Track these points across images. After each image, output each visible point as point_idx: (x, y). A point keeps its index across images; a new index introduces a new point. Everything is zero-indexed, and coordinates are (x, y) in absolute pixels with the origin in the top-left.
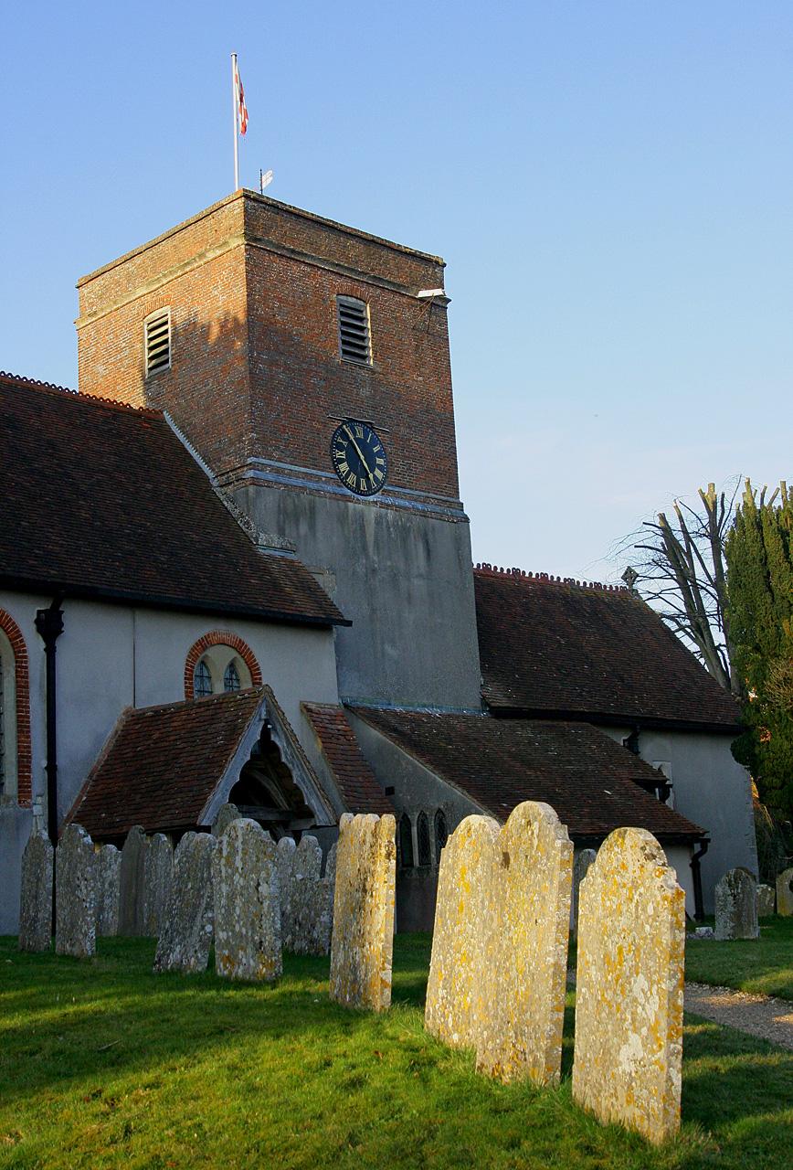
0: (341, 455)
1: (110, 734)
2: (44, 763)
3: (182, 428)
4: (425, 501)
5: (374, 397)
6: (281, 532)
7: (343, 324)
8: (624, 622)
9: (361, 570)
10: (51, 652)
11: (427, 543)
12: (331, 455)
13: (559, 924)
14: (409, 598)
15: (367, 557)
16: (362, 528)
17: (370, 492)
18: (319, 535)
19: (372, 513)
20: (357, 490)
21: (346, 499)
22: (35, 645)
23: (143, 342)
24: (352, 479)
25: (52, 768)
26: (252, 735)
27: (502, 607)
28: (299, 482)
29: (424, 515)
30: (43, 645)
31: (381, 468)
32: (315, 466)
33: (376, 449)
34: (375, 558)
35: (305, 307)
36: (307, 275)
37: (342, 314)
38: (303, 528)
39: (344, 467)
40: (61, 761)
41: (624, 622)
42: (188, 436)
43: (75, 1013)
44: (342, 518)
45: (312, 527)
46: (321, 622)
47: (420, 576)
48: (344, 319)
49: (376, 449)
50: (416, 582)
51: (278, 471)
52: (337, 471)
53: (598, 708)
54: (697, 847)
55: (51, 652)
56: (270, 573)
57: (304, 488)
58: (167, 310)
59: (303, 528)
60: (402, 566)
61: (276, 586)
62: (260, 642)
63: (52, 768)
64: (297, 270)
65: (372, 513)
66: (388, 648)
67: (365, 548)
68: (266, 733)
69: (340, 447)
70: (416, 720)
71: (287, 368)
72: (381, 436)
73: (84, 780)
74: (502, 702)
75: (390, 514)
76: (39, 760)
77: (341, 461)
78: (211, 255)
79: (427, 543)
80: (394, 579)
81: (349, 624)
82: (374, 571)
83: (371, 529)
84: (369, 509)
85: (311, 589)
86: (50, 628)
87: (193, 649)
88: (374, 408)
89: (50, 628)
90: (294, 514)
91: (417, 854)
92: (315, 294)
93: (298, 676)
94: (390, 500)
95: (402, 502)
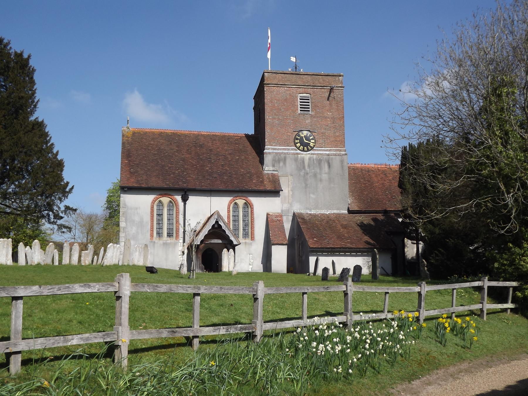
5: (311, 122)
6: (273, 166)
9: (302, 174)
10: (185, 204)
12: (294, 142)
13: (518, 326)
14: (321, 180)
16: (303, 162)
17: (308, 150)
20: (303, 150)
21: (298, 154)
22: (181, 204)
24: (301, 147)
25: (184, 232)
28: (281, 151)
29: (328, 155)
31: (312, 139)
32: (288, 146)
34: (308, 170)
37: (300, 99)
39: (298, 145)
43: (372, 288)
44: (296, 160)
45: (285, 163)
46: (275, 192)
48: (301, 104)
51: (274, 149)
52: (296, 147)
55: (185, 204)
57: (282, 153)
59: (281, 164)
60: (318, 171)
62: (255, 201)
64: (282, 89)
66: (312, 195)
67: (304, 167)
68: (217, 222)
69: (297, 139)
70: (257, 153)
71: (279, 119)
75: (315, 156)
76: (181, 230)
77: (297, 143)
80: (315, 175)
82: (307, 174)
84: (306, 156)
90: (280, 159)
91: (242, 230)
92: (290, 95)
94: (316, 152)
95: (319, 152)
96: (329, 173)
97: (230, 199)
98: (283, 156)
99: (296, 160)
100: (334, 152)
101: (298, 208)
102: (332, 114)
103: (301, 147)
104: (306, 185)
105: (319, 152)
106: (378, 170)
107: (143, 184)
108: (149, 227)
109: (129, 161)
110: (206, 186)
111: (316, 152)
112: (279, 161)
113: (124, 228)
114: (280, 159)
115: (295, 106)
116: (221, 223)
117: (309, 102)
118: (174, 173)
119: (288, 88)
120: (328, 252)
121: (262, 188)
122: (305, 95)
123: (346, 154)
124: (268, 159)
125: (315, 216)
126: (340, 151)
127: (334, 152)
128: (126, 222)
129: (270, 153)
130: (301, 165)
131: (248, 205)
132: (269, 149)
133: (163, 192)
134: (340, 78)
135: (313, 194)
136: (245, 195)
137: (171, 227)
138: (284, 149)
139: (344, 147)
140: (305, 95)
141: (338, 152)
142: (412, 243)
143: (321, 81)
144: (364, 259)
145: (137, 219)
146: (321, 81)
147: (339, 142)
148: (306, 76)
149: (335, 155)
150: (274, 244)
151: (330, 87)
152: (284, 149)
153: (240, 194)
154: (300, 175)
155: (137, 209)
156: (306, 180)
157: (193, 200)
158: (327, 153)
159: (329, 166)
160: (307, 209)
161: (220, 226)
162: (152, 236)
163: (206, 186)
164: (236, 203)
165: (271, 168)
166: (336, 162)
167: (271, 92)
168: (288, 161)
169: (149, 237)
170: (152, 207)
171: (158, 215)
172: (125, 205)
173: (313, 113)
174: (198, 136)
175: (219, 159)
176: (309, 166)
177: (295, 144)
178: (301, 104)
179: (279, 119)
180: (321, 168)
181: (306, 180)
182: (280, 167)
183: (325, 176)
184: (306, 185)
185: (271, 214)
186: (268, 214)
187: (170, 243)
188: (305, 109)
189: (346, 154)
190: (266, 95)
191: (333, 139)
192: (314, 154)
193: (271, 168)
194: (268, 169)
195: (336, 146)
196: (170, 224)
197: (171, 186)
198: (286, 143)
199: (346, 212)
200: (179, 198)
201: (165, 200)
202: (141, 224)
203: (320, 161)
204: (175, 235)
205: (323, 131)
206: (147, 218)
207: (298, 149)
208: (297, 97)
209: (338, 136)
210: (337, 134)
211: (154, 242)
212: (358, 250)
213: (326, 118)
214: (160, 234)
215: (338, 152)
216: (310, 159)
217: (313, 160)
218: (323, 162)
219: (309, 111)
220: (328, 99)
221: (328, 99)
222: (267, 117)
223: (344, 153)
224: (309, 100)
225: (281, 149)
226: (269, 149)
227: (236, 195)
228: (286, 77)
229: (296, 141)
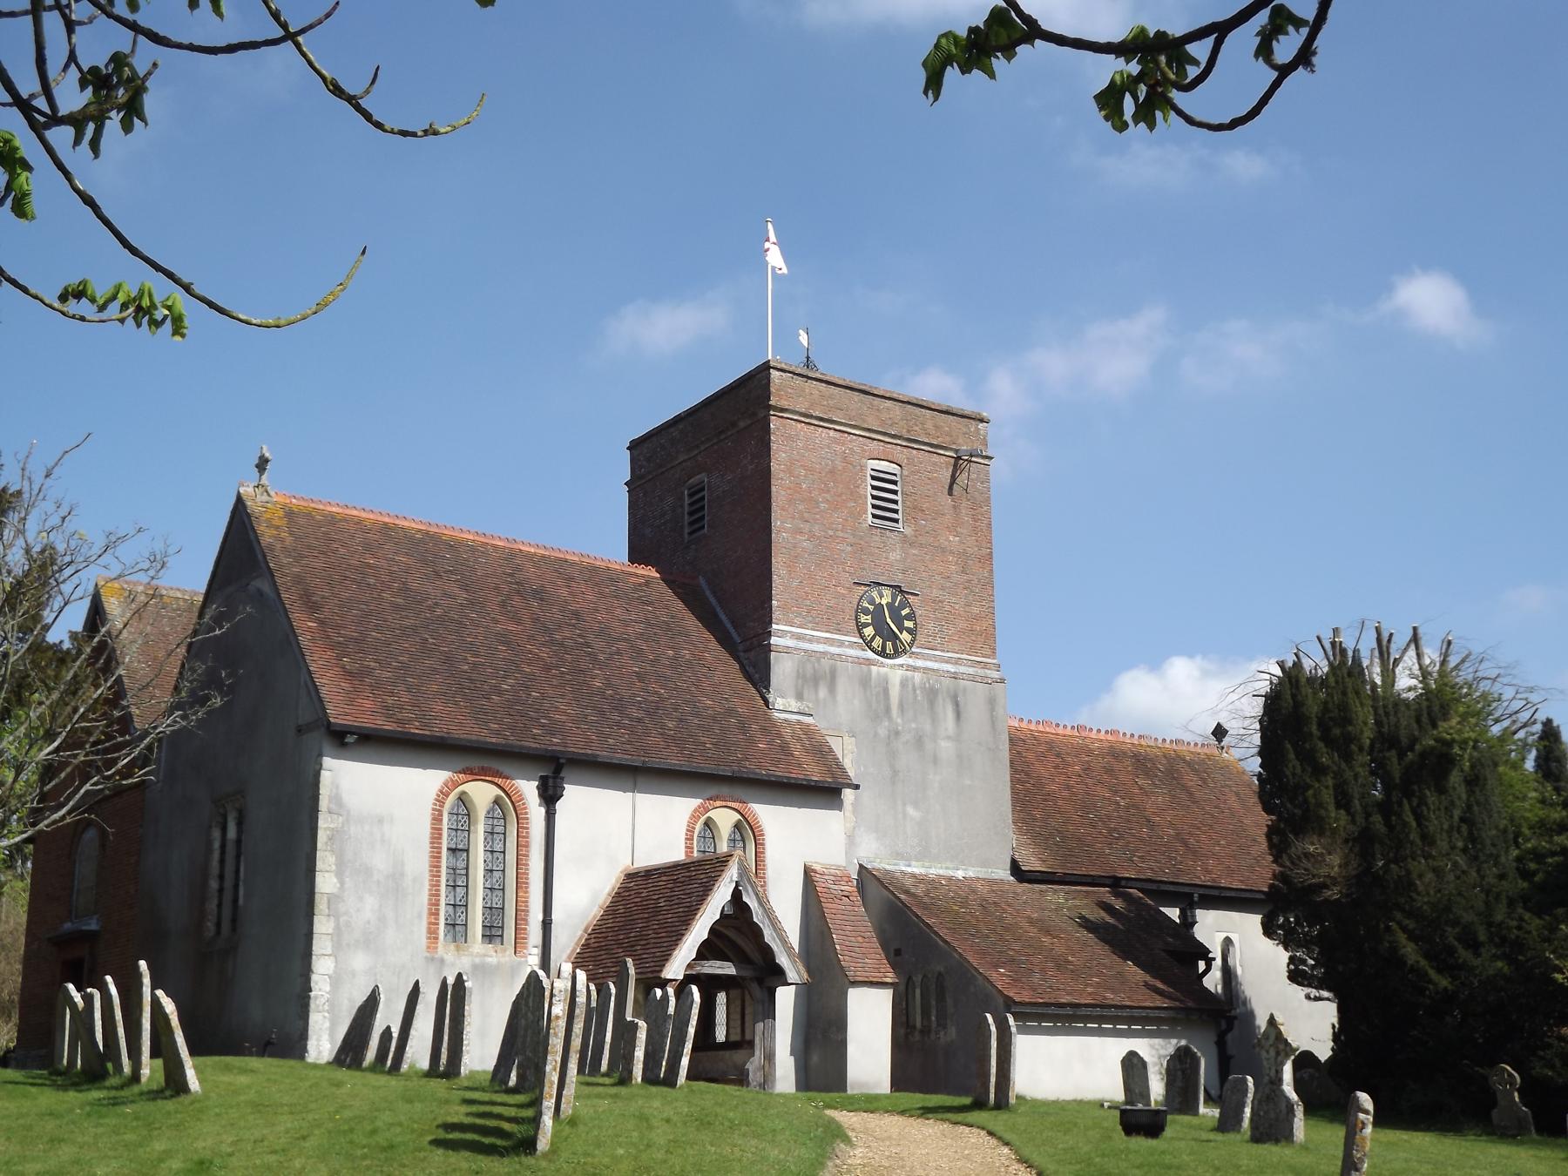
0: (865, 619)
1: (607, 890)
2: (540, 917)
3: (714, 593)
4: (957, 662)
7: (874, 488)
8: (1204, 781)
9: (882, 732)
11: (957, 704)
14: (935, 760)
15: (890, 718)
16: (886, 691)
17: (897, 653)
18: (840, 697)
19: (896, 676)
21: (869, 662)
22: (536, 812)
23: (682, 506)
24: (878, 642)
25: (547, 924)
26: (720, 897)
27: (1057, 767)
28: (820, 648)
29: (955, 676)
30: (543, 810)
31: (909, 631)
32: (839, 631)
33: (904, 613)
35: (832, 472)
36: (835, 441)
37: (873, 478)
38: (823, 692)
39: (869, 631)
40: (556, 915)
41: (1204, 781)
42: (719, 602)
44: (865, 682)
45: (832, 689)
46: (824, 791)
47: (948, 738)
48: (875, 493)
49: (904, 613)
50: (943, 744)
51: (799, 637)
53: (1149, 875)
54: (1224, 1025)
56: (779, 735)
58: (703, 476)
59: (823, 692)
60: (928, 727)
61: (785, 748)
62: (772, 817)
63: (547, 924)
64: (823, 435)
65: (896, 676)
66: (911, 811)
67: (888, 710)
68: (737, 895)
69: (866, 611)
72: (911, 599)
73: (580, 933)
74: (1031, 863)
75: (918, 676)
76: (536, 915)
77: (867, 625)
78: (742, 424)
79: (957, 704)
80: (919, 741)
81: (857, 787)
82: (897, 733)
83: (895, 692)
84: (893, 671)
85: (822, 752)
86: (550, 797)
87: (695, 811)
88: (904, 572)
89: (550, 797)
90: (818, 676)
93: (796, 849)
94: (920, 663)
95: (930, 664)
96: (957, 738)
97: (697, 802)
98: (826, 663)
99: (865, 682)
100: (971, 671)
101: (875, 853)
102: (961, 542)
103: (878, 642)
104: (895, 773)
105: (930, 664)
106: (1035, 738)
107: (410, 721)
108: (424, 898)
109: (321, 622)
110: (625, 752)
111: (920, 663)
112: (815, 680)
113: (332, 899)
114: (818, 676)
115: (856, 496)
116: (749, 900)
117: (895, 492)
118: (500, 693)
119: (838, 435)
120: (1054, 1018)
121: (780, 772)
122: (884, 465)
123: (1002, 681)
124: (782, 670)
125: (932, 884)
126: (985, 666)
127: (971, 671)
128: (340, 874)
129: (787, 650)
130: (877, 699)
131: (746, 830)
132: (783, 634)
133: (476, 763)
134: (981, 426)
135: (916, 805)
136: (739, 791)
137: (496, 903)
138: (827, 641)
139: (993, 654)
140: (884, 465)
141: (981, 672)
142: (1308, 997)
143: (929, 425)
144: (1152, 1047)
145: (379, 862)
146: (929, 425)
147: (980, 636)
148: (889, 403)
149: (973, 679)
150: (855, 984)
151: (957, 451)
152: (827, 641)
153: (725, 790)
154: (876, 734)
155: (381, 821)
156: (892, 755)
157: (577, 798)
158: (951, 668)
159: (958, 715)
160: (899, 856)
161: (746, 909)
162: (432, 934)
163: (625, 752)
164: (463, 799)
165: (794, 705)
166: (975, 700)
167: (790, 438)
168: (842, 684)
169: (424, 941)
170: (437, 819)
171: (453, 851)
172: (337, 799)
173: (908, 531)
174: (512, 558)
175: (618, 653)
176: (901, 706)
177: (860, 627)
178: (875, 493)
179: (812, 536)
180: (934, 720)
181: (892, 755)
182: (817, 700)
183: (946, 748)
184: (895, 773)
185: (817, 867)
186: (808, 872)
187: (498, 967)
188: (885, 511)
189: (1002, 681)
190: (774, 446)
191: (962, 625)
192: (915, 669)
193: (794, 705)
194: (784, 703)
195: (972, 650)
196: (495, 889)
197: (513, 741)
198: (828, 621)
199: (1004, 873)
200: (529, 789)
201: (482, 793)
202: (394, 885)
203: (932, 694)
204: (510, 933)
205: (935, 593)
206: (417, 862)
207: (869, 645)
208: (863, 468)
209: (977, 618)
210: (976, 610)
211: (442, 961)
212: (1136, 1013)
213: (944, 550)
214: (457, 929)
215: (981, 672)
216: (904, 683)
217: (914, 690)
218: (940, 697)
219: (896, 521)
220: (950, 492)
221: (950, 492)
222: (776, 523)
223: (995, 675)
224: (895, 483)
225: (819, 640)
226: (783, 634)
227: (713, 791)
228: (831, 397)
229: (865, 619)
